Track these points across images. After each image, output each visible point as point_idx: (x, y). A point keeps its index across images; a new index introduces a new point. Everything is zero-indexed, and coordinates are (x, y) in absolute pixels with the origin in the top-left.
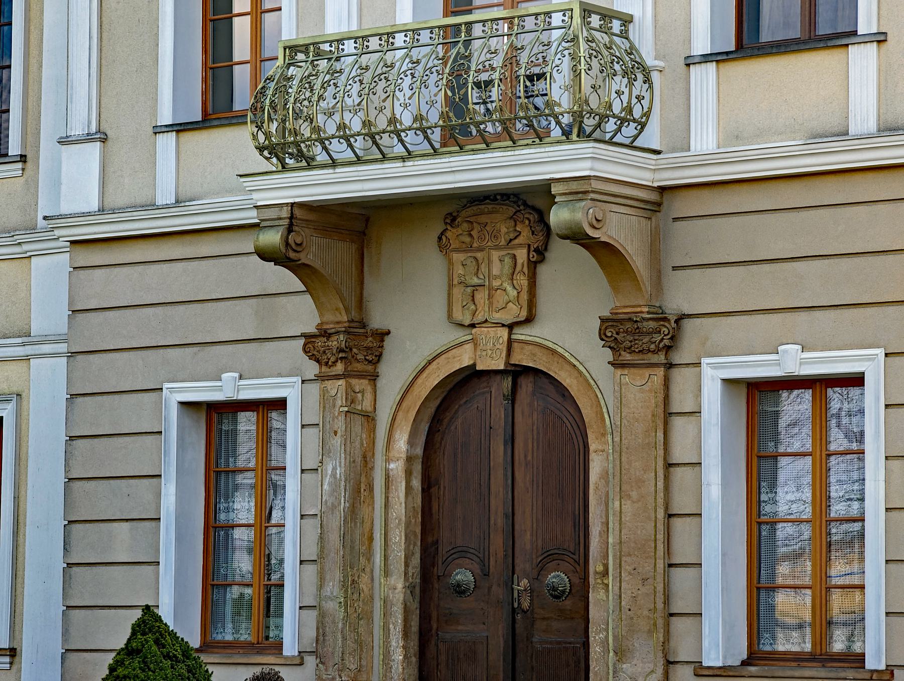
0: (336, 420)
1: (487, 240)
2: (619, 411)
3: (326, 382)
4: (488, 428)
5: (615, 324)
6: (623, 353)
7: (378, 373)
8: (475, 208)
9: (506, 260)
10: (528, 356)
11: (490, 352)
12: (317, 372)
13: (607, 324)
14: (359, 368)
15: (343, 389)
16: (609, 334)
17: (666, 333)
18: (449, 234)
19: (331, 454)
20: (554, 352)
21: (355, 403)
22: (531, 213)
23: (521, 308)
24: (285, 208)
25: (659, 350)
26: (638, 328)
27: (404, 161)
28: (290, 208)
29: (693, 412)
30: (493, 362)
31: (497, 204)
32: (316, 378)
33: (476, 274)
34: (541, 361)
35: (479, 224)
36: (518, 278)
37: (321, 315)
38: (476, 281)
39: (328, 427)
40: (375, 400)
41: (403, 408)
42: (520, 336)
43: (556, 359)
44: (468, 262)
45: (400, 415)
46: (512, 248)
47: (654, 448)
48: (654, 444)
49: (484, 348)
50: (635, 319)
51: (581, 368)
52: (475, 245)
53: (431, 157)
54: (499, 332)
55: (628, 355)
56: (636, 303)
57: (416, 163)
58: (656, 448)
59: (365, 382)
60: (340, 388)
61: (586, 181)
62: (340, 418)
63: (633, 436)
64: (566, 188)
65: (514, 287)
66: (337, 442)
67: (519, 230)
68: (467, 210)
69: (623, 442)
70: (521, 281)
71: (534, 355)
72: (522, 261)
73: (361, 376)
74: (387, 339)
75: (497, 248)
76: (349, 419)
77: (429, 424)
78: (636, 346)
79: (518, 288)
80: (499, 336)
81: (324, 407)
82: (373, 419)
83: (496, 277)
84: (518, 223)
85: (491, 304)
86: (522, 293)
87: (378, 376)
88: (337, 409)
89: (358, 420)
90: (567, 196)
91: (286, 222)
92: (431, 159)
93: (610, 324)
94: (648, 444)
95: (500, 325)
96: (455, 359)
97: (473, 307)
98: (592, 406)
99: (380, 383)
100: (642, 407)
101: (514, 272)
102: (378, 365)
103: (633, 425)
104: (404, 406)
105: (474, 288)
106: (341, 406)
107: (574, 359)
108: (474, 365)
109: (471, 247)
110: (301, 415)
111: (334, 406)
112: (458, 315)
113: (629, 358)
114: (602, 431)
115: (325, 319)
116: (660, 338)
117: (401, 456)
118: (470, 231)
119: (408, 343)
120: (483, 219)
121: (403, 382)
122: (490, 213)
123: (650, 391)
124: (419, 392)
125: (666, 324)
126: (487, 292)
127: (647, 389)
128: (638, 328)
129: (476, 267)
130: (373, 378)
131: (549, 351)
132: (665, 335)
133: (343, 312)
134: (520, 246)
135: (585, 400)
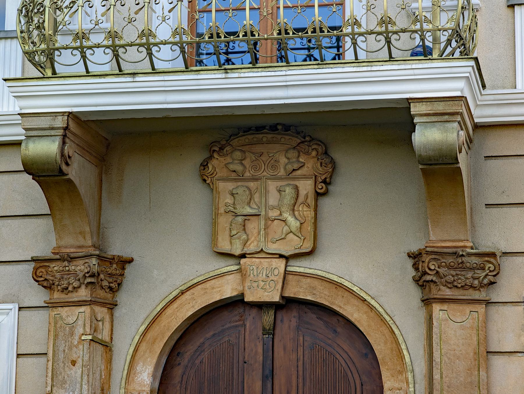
0: (75, 349)
1: (263, 170)
2: (439, 347)
3: (60, 308)
4: (241, 362)
5: (437, 257)
6: (442, 287)
7: (117, 301)
8: (250, 137)
9: (287, 191)
10: (306, 289)
11: (262, 284)
12: (47, 299)
13: (431, 257)
14: (102, 295)
15: (88, 314)
16: (432, 267)
17: (492, 268)
18: (214, 162)
19: (67, 386)
20: (339, 286)
21: (97, 332)
22: (319, 145)
23: (304, 239)
24: (60, 118)
25: (482, 287)
26: (462, 262)
27: (227, 73)
28: (66, 118)
29: (515, 352)
30: (266, 293)
31: (279, 134)
32: (46, 305)
33: (249, 204)
34: (323, 295)
35: (253, 153)
36: (301, 209)
37: (59, 237)
38: (248, 210)
39: (61, 356)
40: (112, 330)
41: (148, 339)
42: (297, 268)
43: (340, 293)
44: (240, 191)
45: (143, 346)
46: (294, 179)
47: (477, 388)
48: (476, 383)
49: (255, 279)
50: (461, 253)
51: (373, 302)
52: (247, 174)
53: (263, 69)
54: (274, 263)
55: (448, 290)
56: (457, 237)
57: (242, 75)
58: (479, 387)
59: (105, 310)
60: (82, 316)
61: (455, 102)
62: (81, 347)
63: (455, 375)
64: (430, 108)
65: (296, 218)
66: (76, 373)
67: (303, 161)
68: (241, 138)
69: (444, 379)
70: (305, 212)
71: (314, 288)
72: (305, 192)
73: (103, 304)
74: (129, 269)
75: (275, 178)
76: (92, 349)
77: (167, 357)
78: (460, 281)
79: (300, 219)
80: (274, 267)
81: (56, 336)
82: (110, 350)
83: (273, 208)
84: (301, 153)
85: (266, 235)
86: (305, 225)
87: (116, 305)
88: (77, 337)
89: (100, 348)
90: (429, 117)
91: (61, 132)
92: (262, 71)
93: (433, 256)
94: (471, 383)
95: (277, 256)
96: (215, 290)
97: (245, 236)
98: (386, 343)
99: (117, 313)
100: (463, 345)
101: (295, 203)
102: (116, 294)
103: (454, 363)
104: (149, 337)
105: (246, 218)
106: (83, 334)
107: (365, 293)
108: (242, 295)
109: (242, 176)
110: (17, 343)
111: (72, 334)
112: (225, 246)
113: (449, 293)
114: (399, 368)
115: (62, 243)
116: (484, 274)
117: (143, 389)
118: (242, 160)
119: (155, 272)
120: (258, 148)
121: (148, 312)
122: (269, 142)
123: (472, 328)
124: (169, 323)
125: (492, 260)
126: (263, 223)
127: (468, 326)
128: (462, 262)
129: (249, 197)
130: (111, 306)
131: (331, 284)
132: (490, 271)
133: (88, 237)
134: (305, 177)
135: (377, 335)
